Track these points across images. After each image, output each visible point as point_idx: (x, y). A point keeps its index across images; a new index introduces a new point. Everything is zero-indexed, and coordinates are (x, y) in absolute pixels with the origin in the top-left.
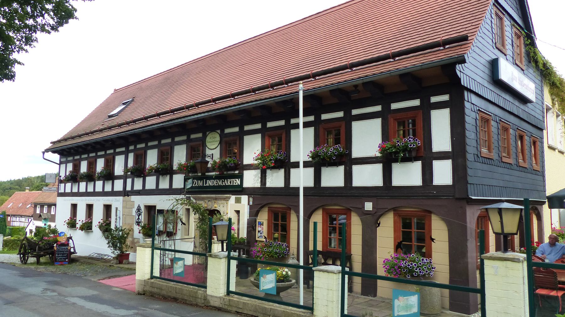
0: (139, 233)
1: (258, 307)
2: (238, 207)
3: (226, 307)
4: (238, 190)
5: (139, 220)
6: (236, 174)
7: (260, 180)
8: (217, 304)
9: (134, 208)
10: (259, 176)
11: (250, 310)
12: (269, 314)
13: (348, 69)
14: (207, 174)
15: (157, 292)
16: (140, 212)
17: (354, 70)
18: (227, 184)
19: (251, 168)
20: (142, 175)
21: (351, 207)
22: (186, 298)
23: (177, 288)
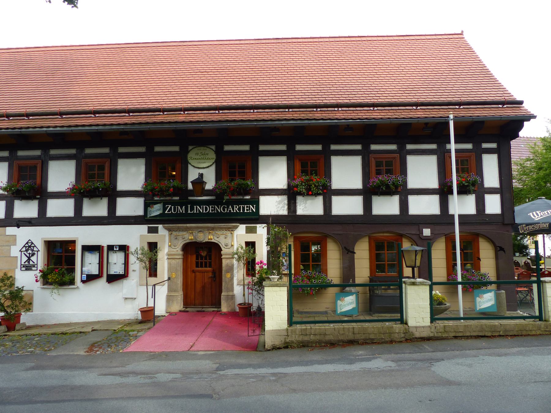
0: (37, 281)
1: (484, 327)
2: (251, 238)
3: (440, 334)
4: (252, 218)
5: (31, 263)
6: (247, 199)
7: (286, 207)
8: (425, 334)
9: (15, 244)
10: (284, 203)
11: (474, 331)
12: (499, 330)
13: (58, 115)
14: (190, 198)
15: (314, 340)
16: (33, 250)
17: (31, 119)
18: (232, 211)
19: (272, 193)
20: (39, 197)
21: (406, 234)
22: (372, 336)
23: (355, 329)
